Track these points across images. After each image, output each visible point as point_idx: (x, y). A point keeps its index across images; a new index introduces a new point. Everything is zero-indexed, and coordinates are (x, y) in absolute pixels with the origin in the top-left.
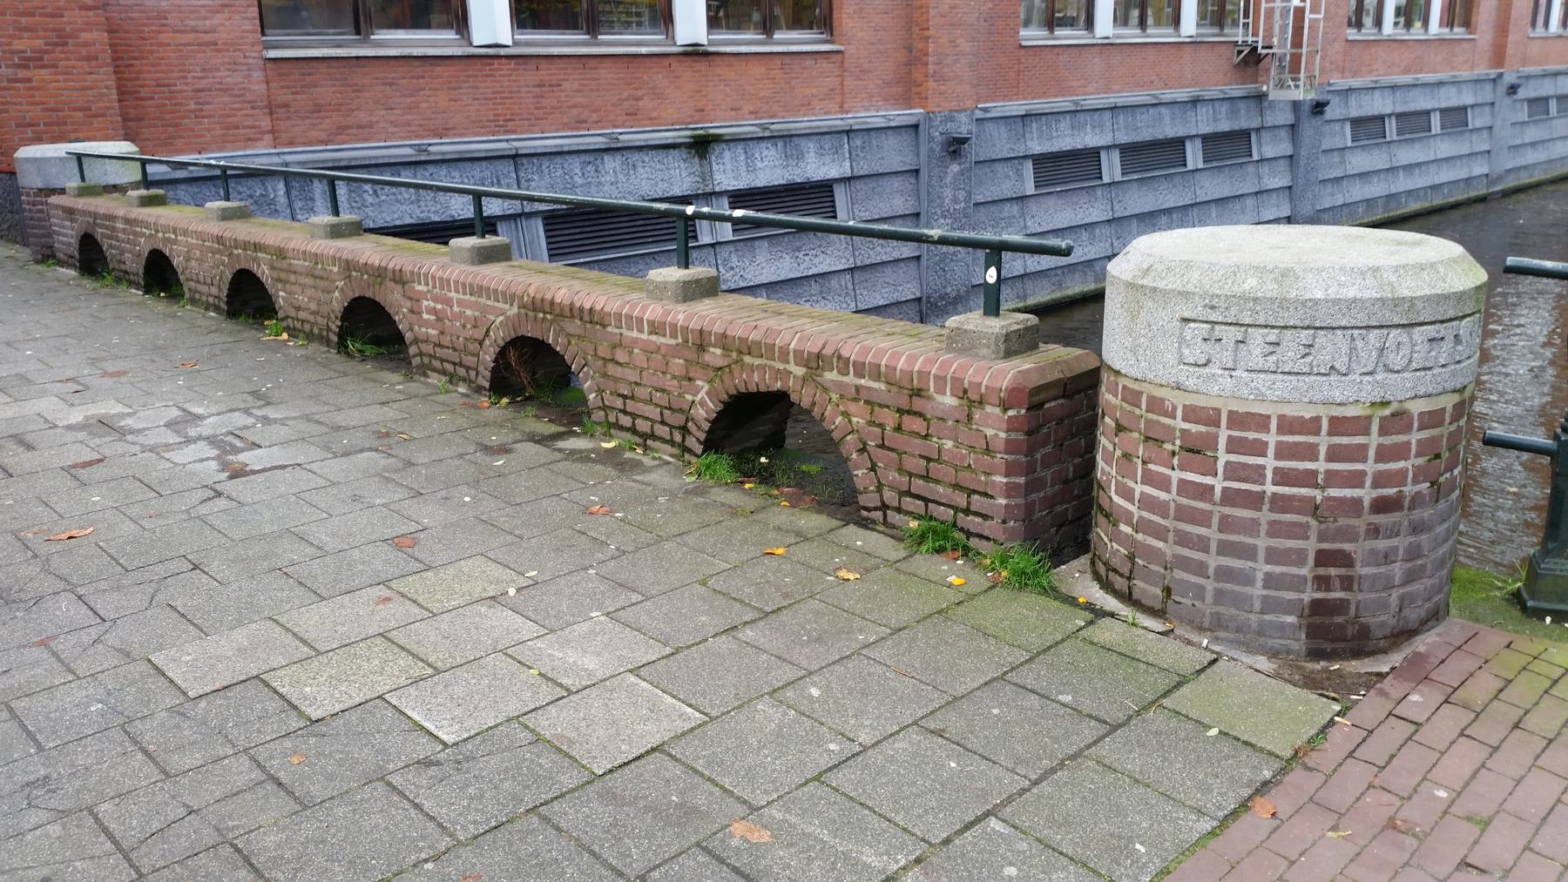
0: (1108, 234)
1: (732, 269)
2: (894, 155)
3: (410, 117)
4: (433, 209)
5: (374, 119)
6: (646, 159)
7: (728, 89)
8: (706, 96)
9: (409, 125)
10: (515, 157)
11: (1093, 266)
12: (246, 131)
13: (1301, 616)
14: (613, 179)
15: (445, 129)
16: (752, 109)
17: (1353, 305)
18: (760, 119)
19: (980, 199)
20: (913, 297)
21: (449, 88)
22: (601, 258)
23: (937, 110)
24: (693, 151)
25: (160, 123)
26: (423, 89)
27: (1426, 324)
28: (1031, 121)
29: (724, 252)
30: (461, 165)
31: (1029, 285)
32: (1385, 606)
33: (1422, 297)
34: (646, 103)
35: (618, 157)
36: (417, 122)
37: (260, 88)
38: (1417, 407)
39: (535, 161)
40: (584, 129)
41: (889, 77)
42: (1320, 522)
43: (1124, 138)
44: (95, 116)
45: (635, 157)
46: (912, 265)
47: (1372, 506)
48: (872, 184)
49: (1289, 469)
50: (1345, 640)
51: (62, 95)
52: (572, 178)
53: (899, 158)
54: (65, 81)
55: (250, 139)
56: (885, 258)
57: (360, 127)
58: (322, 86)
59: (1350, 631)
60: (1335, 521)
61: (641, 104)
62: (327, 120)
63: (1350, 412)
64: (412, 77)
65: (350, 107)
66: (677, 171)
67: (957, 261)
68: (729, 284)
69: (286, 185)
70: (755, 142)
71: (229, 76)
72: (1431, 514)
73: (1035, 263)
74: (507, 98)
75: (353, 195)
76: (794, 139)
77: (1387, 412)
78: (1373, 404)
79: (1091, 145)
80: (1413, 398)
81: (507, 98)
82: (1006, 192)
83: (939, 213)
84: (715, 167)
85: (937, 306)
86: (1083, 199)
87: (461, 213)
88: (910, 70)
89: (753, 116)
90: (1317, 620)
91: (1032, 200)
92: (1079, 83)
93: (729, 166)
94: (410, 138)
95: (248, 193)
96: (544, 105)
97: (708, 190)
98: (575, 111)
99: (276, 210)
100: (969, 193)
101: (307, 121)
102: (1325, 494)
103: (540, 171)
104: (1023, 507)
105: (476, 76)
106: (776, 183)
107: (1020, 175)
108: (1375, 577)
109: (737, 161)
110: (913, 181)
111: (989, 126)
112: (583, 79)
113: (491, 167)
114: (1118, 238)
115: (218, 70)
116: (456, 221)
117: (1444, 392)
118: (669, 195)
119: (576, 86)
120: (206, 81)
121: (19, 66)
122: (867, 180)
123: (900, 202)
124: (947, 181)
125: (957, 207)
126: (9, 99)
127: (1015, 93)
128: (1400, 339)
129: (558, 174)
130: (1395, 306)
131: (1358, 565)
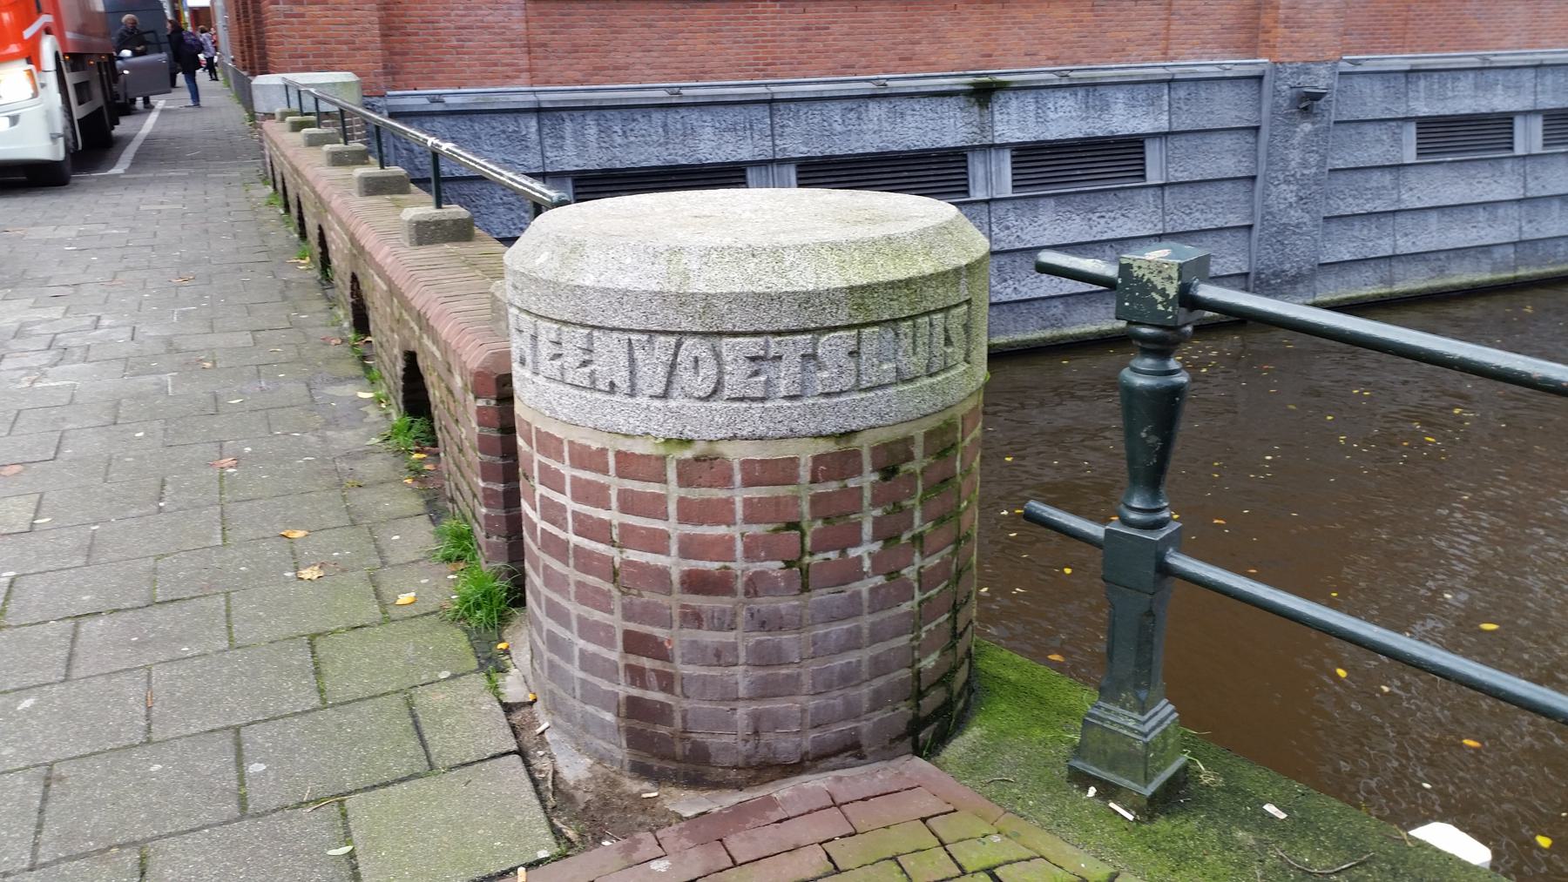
0: (1516, 215)
1: (1008, 228)
2: (1227, 109)
3: (666, 60)
4: (681, 152)
5: (630, 60)
6: (917, 107)
7: (1022, 33)
8: (996, 40)
10: (771, 102)
11: (1491, 252)
12: (505, 68)
13: (618, 715)
14: (876, 128)
15: (702, 72)
16: (1050, 54)
17: (625, 298)
18: (1060, 65)
19: (1340, 164)
20: (1238, 271)
21: (709, 31)
23: (1288, 60)
24: (973, 100)
25: (423, 57)
26: (682, 32)
27: (744, 334)
28: (1419, 78)
29: (999, 210)
30: (712, 108)
31: (1399, 269)
32: (727, 724)
33: (725, 295)
34: (923, 48)
35: (885, 105)
36: (674, 65)
37: (521, 27)
38: (736, 453)
39: (792, 106)
40: (851, 74)
41: (1230, 22)
42: (623, 593)
43: (1549, 102)
44: (359, 49)
45: (904, 105)
46: (1242, 235)
47: (683, 583)
48: (1195, 140)
49: (585, 515)
50: (674, 759)
51: (330, 29)
52: (830, 125)
53: (1234, 113)
54: (334, 16)
55: (508, 77)
56: (1204, 226)
57: (616, 68)
58: (580, 27)
59: (679, 749)
60: (640, 595)
61: (917, 48)
63: (639, 448)
64: (672, 20)
65: (607, 48)
66: (952, 120)
67: (1302, 234)
68: (1002, 244)
69: (539, 123)
70: (1049, 90)
71: (491, 14)
72: (794, 607)
73: (1409, 244)
74: (769, 41)
75: (603, 135)
76: (1098, 88)
77: (688, 454)
78: (668, 441)
79: (1501, 109)
80: (730, 439)
81: (769, 41)
82: (1376, 158)
83: (1281, 177)
84: (997, 117)
85: (1269, 285)
86: (1484, 172)
87: (709, 157)
88: (1259, 14)
89: (1051, 62)
90: (638, 725)
91: (1412, 170)
92: (1491, 35)
93: (1014, 117)
94: (665, 80)
95: (502, 128)
96: (809, 49)
97: (986, 141)
98: (842, 55)
99: (527, 147)
100: (1324, 158)
101: (563, 61)
102: (624, 556)
103: (796, 116)
104: (504, 520)
105: (738, 19)
106: (1071, 136)
107: (1397, 141)
108: (704, 681)
109: (1024, 111)
110: (1251, 139)
111: (1358, 82)
112: (854, 22)
113: (746, 111)
114: (1530, 222)
115: (480, 8)
116: (704, 165)
117: (793, 435)
118: (938, 146)
119: (846, 28)
120: (468, 19)
122: (1190, 137)
123: (1230, 163)
124: (1295, 142)
125: (1306, 172)
126: (284, 33)
127: (1399, 43)
128: (695, 353)
129: (816, 121)
130: (682, 304)
131: (678, 661)
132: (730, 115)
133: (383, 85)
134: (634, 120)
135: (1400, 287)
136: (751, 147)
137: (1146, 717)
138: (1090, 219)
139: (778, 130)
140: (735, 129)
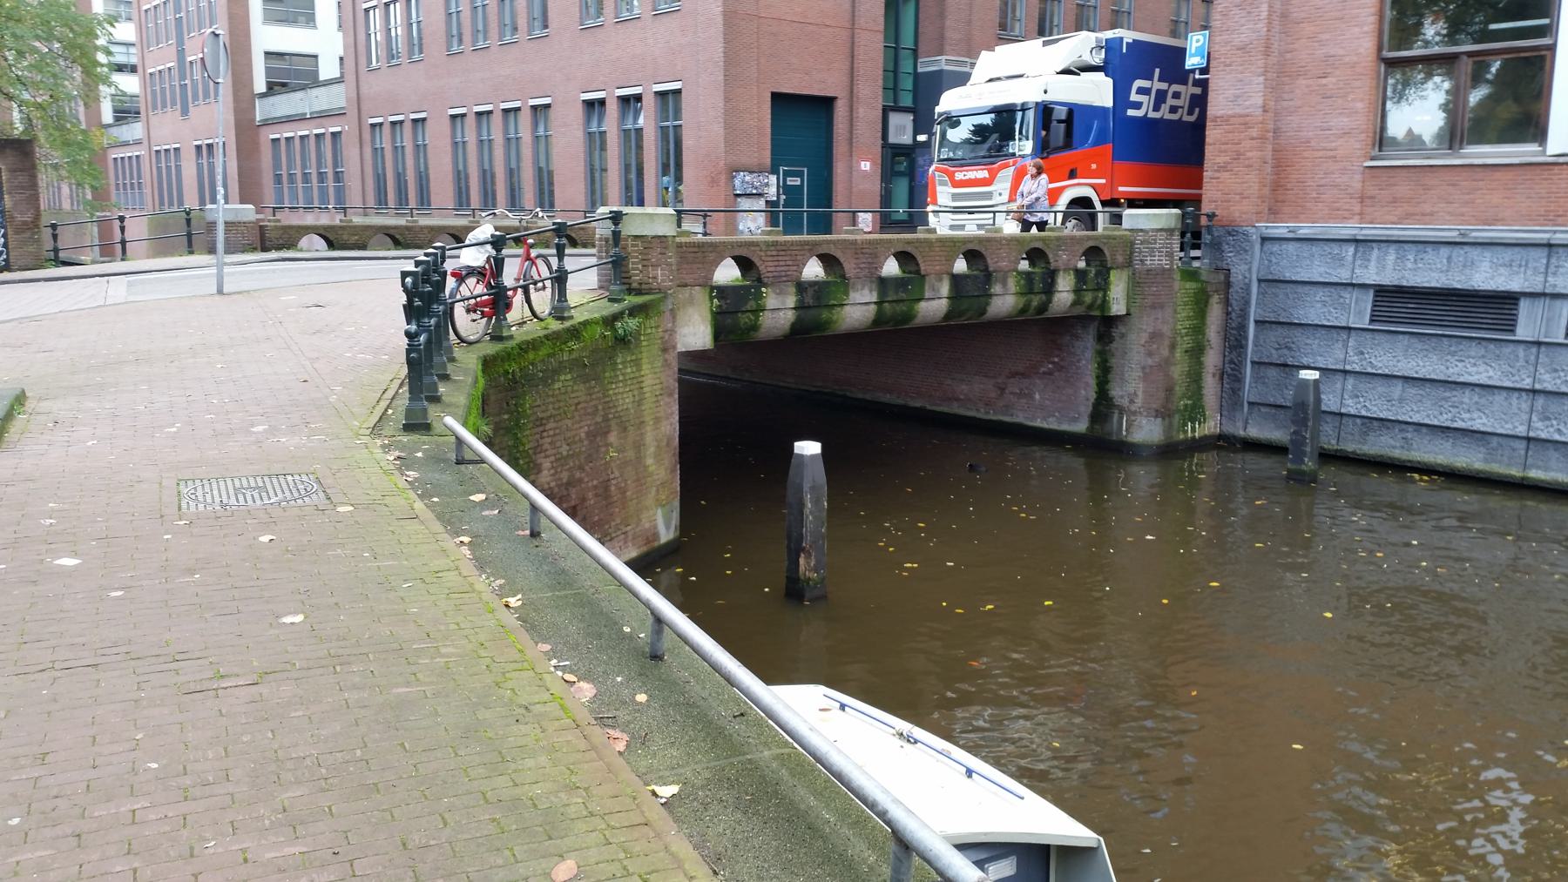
3: (1464, 210)
5: (1435, 209)
9: (1463, 215)
10: (1549, 246)
22: (1474, 335)
30: (1493, 248)
37: (1358, 186)
57: (1423, 215)
62: (1400, 209)
64: (1474, 180)
101: (1386, 209)
121: (1216, 171)
132: (1508, 254)
133: (1254, 219)
134: (1425, 252)
135: (1535, 474)
136: (1522, 281)
137: (102, 259)
138: (1448, 361)
139: (1552, 269)
140: (1511, 265)
